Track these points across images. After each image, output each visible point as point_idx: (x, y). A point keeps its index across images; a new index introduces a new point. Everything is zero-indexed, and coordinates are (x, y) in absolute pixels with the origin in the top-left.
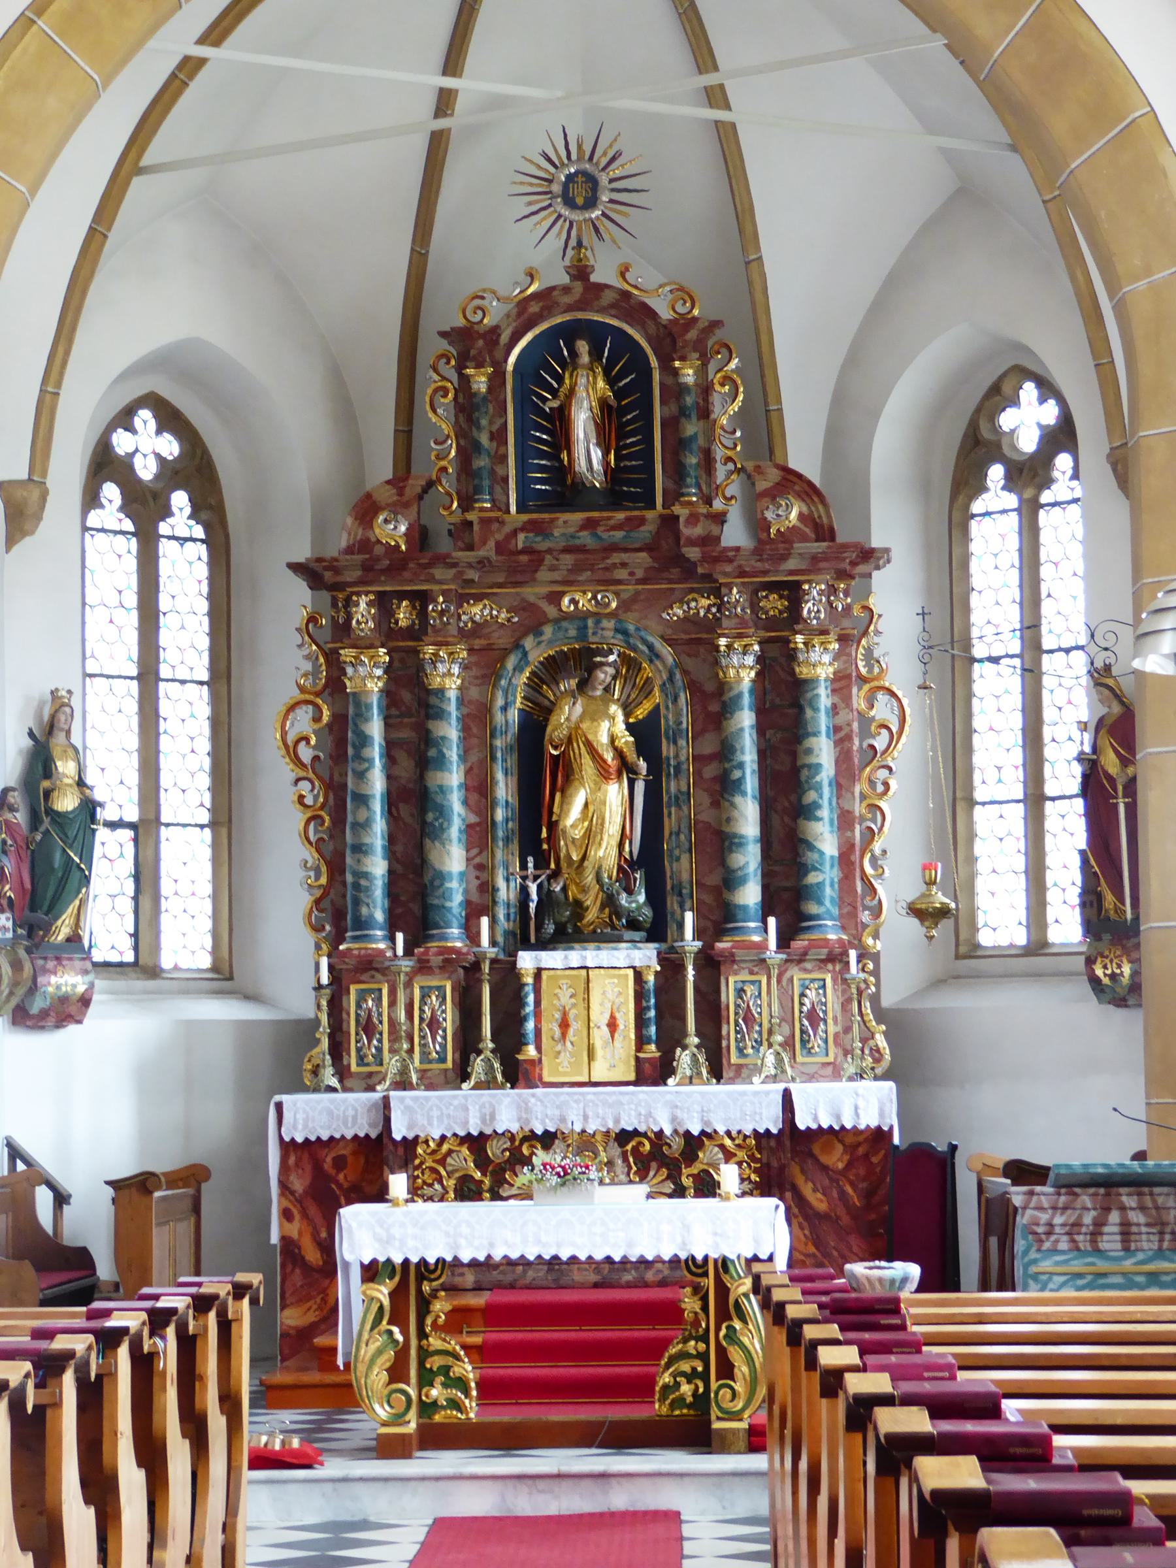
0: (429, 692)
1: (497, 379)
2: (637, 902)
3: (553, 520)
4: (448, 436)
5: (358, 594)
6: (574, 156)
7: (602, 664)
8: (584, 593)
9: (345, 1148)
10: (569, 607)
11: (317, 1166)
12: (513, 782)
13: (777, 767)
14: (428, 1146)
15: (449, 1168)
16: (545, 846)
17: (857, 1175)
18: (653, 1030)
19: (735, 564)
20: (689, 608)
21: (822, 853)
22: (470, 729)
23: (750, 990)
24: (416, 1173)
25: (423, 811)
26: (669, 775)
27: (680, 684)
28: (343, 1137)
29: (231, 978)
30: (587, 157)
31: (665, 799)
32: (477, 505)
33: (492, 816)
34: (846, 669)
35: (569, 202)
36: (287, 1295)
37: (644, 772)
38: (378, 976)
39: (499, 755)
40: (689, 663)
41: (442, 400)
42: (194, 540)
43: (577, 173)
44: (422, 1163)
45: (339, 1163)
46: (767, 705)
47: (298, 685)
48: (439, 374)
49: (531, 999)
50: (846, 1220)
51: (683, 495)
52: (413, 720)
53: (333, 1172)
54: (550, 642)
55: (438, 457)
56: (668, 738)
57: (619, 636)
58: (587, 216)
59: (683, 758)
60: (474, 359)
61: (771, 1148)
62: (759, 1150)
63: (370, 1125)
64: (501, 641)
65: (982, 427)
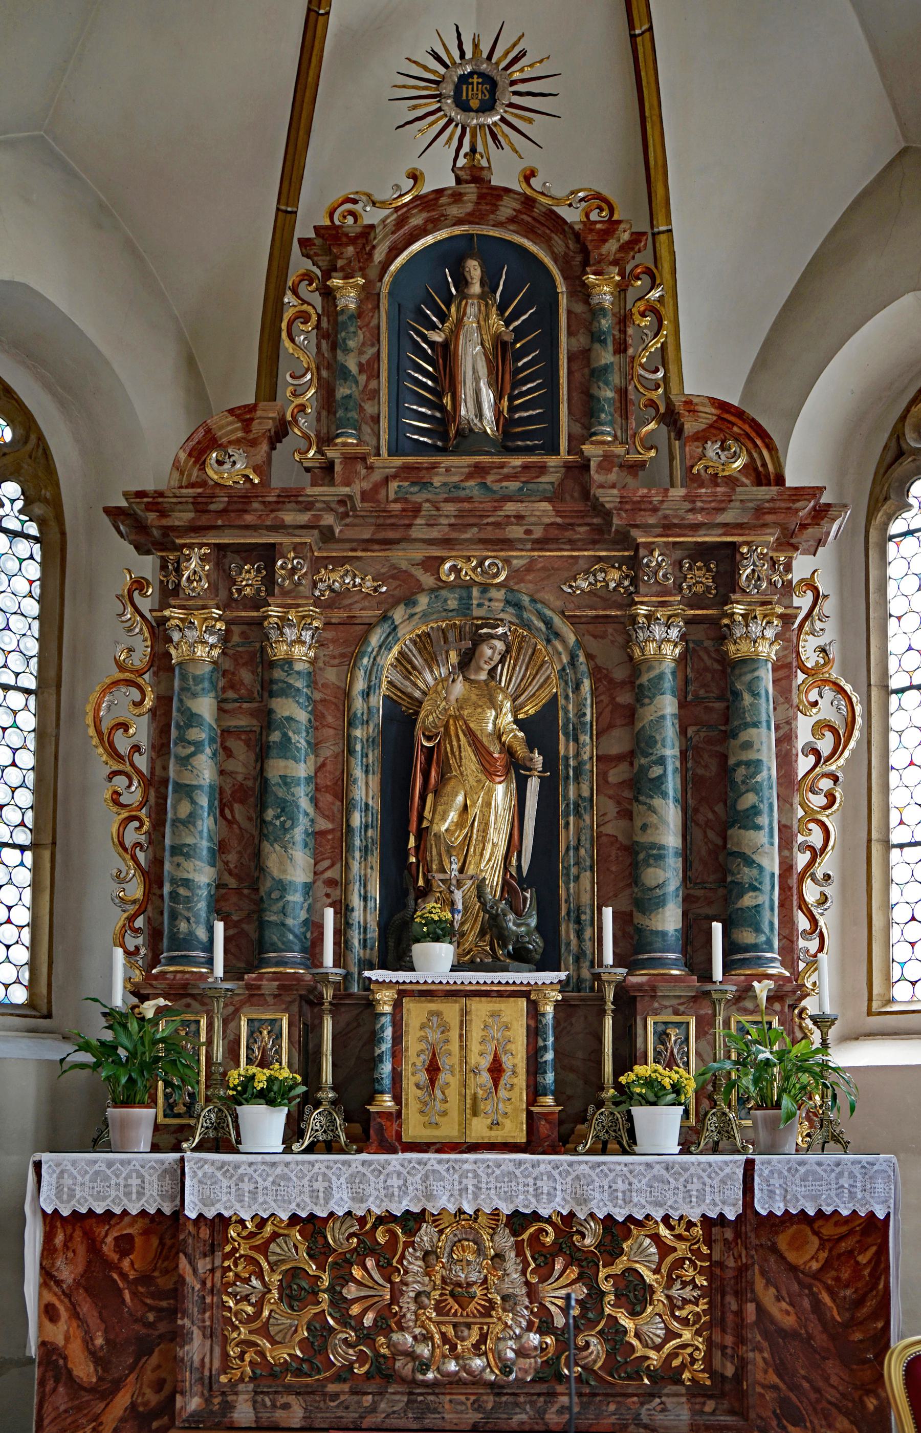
0: (272, 665)
1: (369, 295)
2: (528, 925)
3: (433, 467)
4: (307, 370)
5: (190, 546)
6: (469, 55)
7: (492, 636)
8: (468, 559)
9: (131, 1225)
10: (448, 575)
11: (94, 1248)
12: (374, 781)
13: (700, 771)
14: (245, 1227)
15: (272, 1258)
16: (413, 859)
17: (837, 1279)
18: (550, 1077)
19: (660, 513)
20: (596, 581)
21: (761, 868)
22: (323, 716)
23: (673, 1033)
24: (226, 1264)
25: (262, 807)
26: (567, 777)
27: (583, 668)
28: (125, 1213)
29: (49, 1016)
30: (485, 55)
31: (562, 807)
32: (339, 440)
33: (347, 821)
34: (785, 656)
35: (463, 106)
36: (46, 1422)
37: (539, 767)
38: (195, 1005)
39: (358, 747)
40: (594, 645)
41: (302, 327)
42: (27, 537)
43: (471, 74)
44: (235, 1250)
45: (125, 1245)
46: (690, 698)
47: (117, 662)
48: (298, 297)
49: (388, 1033)
50: (821, 1339)
51: (595, 434)
52: (255, 705)
53: (115, 1257)
54: (425, 615)
55: (295, 394)
56: (566, 735)
57: (510, 610)
58: (482, 120)
59: (586, 757)
60: (342, 269)
61: (726, 1240)
62: (709, 1242)
63: (162, 1197)
64: (364, 614)
65: (907, 437)
